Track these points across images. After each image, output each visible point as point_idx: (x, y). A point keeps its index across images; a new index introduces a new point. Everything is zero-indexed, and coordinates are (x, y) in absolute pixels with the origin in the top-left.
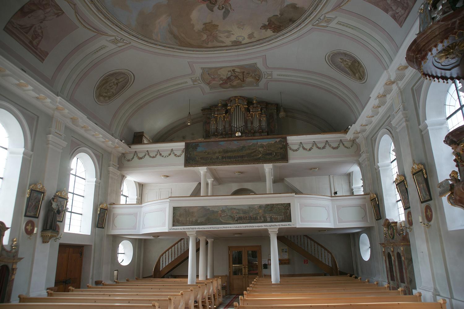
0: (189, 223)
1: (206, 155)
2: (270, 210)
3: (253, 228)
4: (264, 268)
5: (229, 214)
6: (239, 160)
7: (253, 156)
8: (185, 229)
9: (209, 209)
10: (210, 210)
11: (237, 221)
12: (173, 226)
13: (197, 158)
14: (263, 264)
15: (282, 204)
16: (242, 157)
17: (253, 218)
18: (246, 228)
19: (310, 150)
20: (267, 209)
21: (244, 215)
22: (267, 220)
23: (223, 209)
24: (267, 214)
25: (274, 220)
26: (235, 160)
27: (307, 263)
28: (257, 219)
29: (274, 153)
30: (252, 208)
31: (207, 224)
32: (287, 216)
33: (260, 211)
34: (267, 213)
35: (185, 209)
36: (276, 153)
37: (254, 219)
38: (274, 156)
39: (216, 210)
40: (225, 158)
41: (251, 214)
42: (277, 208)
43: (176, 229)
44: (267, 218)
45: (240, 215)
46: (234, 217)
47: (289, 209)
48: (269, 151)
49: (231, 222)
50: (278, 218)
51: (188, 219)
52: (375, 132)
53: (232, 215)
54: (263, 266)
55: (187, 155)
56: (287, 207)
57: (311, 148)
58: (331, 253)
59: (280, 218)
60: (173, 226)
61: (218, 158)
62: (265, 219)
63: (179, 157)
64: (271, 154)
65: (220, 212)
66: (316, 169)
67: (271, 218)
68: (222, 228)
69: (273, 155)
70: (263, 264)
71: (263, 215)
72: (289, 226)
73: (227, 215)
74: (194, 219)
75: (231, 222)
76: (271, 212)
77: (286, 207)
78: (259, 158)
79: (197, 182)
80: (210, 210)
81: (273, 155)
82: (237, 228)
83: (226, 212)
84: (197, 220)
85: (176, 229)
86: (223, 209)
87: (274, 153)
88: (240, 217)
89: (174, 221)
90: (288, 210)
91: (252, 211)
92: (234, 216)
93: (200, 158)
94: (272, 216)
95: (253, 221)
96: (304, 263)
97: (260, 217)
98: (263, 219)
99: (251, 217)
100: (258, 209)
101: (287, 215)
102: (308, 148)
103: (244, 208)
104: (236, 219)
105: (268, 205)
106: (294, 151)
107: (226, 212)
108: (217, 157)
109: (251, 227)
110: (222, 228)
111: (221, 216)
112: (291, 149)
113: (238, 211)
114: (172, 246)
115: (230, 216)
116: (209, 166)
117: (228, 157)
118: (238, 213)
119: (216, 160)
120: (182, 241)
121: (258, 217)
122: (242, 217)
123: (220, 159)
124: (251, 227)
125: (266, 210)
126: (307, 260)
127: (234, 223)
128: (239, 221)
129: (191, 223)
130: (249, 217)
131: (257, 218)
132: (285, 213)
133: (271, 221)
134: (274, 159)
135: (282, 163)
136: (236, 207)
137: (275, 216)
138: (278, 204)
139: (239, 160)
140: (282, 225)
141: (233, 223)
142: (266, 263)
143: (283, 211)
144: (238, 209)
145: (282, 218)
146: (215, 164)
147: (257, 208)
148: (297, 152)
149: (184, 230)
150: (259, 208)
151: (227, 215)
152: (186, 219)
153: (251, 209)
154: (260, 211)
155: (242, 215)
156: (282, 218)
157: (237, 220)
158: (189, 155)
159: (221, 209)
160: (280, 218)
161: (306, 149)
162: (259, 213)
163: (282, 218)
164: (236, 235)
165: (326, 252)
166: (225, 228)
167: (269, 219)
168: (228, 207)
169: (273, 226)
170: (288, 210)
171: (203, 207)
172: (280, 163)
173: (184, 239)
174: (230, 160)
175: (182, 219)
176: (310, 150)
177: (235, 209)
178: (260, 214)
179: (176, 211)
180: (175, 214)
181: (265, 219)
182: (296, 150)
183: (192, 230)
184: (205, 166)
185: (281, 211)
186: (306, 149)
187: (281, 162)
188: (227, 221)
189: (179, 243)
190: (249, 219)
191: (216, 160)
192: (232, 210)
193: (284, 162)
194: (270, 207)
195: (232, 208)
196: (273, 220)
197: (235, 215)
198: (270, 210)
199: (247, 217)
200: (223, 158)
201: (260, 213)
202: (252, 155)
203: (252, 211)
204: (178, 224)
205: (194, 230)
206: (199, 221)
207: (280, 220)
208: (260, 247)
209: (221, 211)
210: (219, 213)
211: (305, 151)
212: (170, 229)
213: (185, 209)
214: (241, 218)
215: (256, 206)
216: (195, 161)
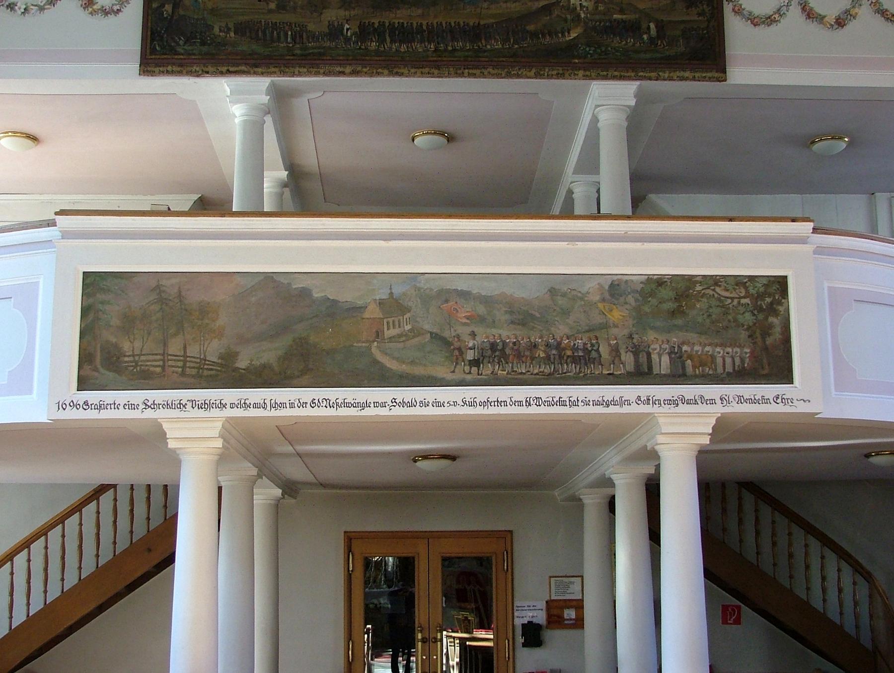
0: (183, 374)
1: (270, 11)
2: (673, 313)
3: (575, 410)
4: (525, 645)
5: (427, 327)
6: (454, 50)
7: (534, 35)
8: (154, 406)
9: (305, 293)
10: (317, 295)
11: (475, 370)
12: (83, 384)
13: (216, 30)
14: (518, 622)
15: (740, 282)
16: (475, 33)
17: (569, 353)
18: (533, 410)
19: (840, 23)
20: (654, 301)
21: (518, 333)
22: (656, 371)
23: (391, 294)
24: (651, 336)
25: (694, 367)
26: (436, 50)
27: (738, 622)
28: (598, 361)
29: (652, 26)
30: (564, 295)
31: (295, 382)
32: (766, 349)
33: (616, 315)
34: (653, 328)
35: (158, 287)
36: (660, 26)
37: (575, 360)
38: (651, 39)
39: (347, 296)
40: (379, 33)
41: (561, 330)
42: (714, 303)
43: (100, 407)
44: (655, 357)
45: (494, 331)
46: (457, 345)
47: (781, 308)
48: (622, 11)
49: (442, 372)
50: (719, 361)
51: (174, 347)
52: (638, 245)
53: (447, 334)
54: (519, 631)
55: (155, 5)
56: (768, 300)
57: (847, 12)
58: (868, 577)
59: (728, 360)
60: (83, 384)
61: (335, 32)
62: (643, 358)
63: (111, 17)
64: (633, 28)
65: (372, 312)
66: (841, 138)
67: (677, 357)
68: (383, 405)
69: (645, 37)
70: (518, 622)
71: (631, 337)
72: (780, 408)
73: (416, 332)
74: (213, 350)
75: (442, 372)
76: (679, 322)
77: (760, 296)
78: (571, 47)
79: (192, 192)
80: (317, 295)
81: (645, 37)
82: (479, 410)
83: (409, 310)
84: (229, 357)
85: (100, 407)
86: (391, 294)
87: (652, 26)
88: (493, 346)
89: (85, 358)
90: (776, 313)
91: (566, 313)
92: (458, 336)
93: (231, 25)
94: (685, 348)
95: (573, 369)
96: (725, 622)
97: (615, 351)
98: (628, 358)
99: (558, 346)
100: (603, 300)
101: (769, 341)
102: (831, 12)
103: (520, 294)
104: (470, 355)
105: (659, 282)
106: (755, 21)
107: (409, 310)
108: (330, 24)
109: (561, 403)
110: (383, 405)
111: (378, 334)
112: (738, 11)
113: (481, 310)
114: (52, 526)
115: (435, 336)
116: (283, 73)
117: (392, 28)
118: (481, 320)
119: (328, 44)
120: (106, 499)
121: (604, 350)
122: (504, 343)
123: (347, 40)
124: (561, 403)
125: (647, 309)
126: (739, 607)
127: (458, 376)
128: (487, 370)
129: (194, 371)
130: (548, 345)
131: (594, 354)
132: (758, 334)
133: (678, 377)
134: (648, 56)
135: (694, 79)
136: (476, 288)
137: (697, 348)
138: (716, 281)
139: (454, 50)
140: (740, 399)
141: (449, 377)
142: (535, 621)
143: (748, 318)
144: (487, 301)
145: (737, 361)
146: (318, 66)
147: (597, 298)
148: (773, 27)
149: (149, 414)
150: (607, 296)
151: (416, 332)
152: (165, 345)
153: (561, 301)
154: (616, 315)
155: (506, 334)
156: (742, 360)
157: (476, 363)
158: (168, 8)
159: (383, 294)
160: (728, 360)
161: (820, 19)
162: (605, 326)
163: (737, 361)
164: (423, 464)
165: (847, 570)
166: (403, 404)
167: (665, 359)
168: (422, 284)
169: (689, 402)
170: (776, 313)
171: (269, 277)
172: (682, 79)
173: (114, 486)
174: (403, 48)
175: (138, 344)
176: (840, 23)
177: (464, 295)
178: (614, 331)
179: (100, 297)
180: (91, 316)
181: (643, 358)
182: (769, 20)
183: (201, 413)
184: (262, 74)
185: (735, 320)
186: (820, 19)
187: (687, 74)
188: (413, 363)
189: (72, 522)
190: (548, 357)
191: (328, 44)
192: (447, 301)
193: (704, 79)
194: (672, 294)
195: (448, 291)
196: (689, 370)
197: (464, 331)
198: (673, 313)
199: (535, 346)
200: (364, 32)
201: (616, 326)
202: (531, 28)
203: (566, 313)
204: (111, 375)
205: (215, 412)
206: (242, 363)
207: (729, 368)
208: (506, 537)
209: (381, 303)
210: (367, 315)
211: (813, 27)
212: (62, 406)
213: (158, 287)
214: (503, 350)
215: (592, 285)
216: (203, 43)
